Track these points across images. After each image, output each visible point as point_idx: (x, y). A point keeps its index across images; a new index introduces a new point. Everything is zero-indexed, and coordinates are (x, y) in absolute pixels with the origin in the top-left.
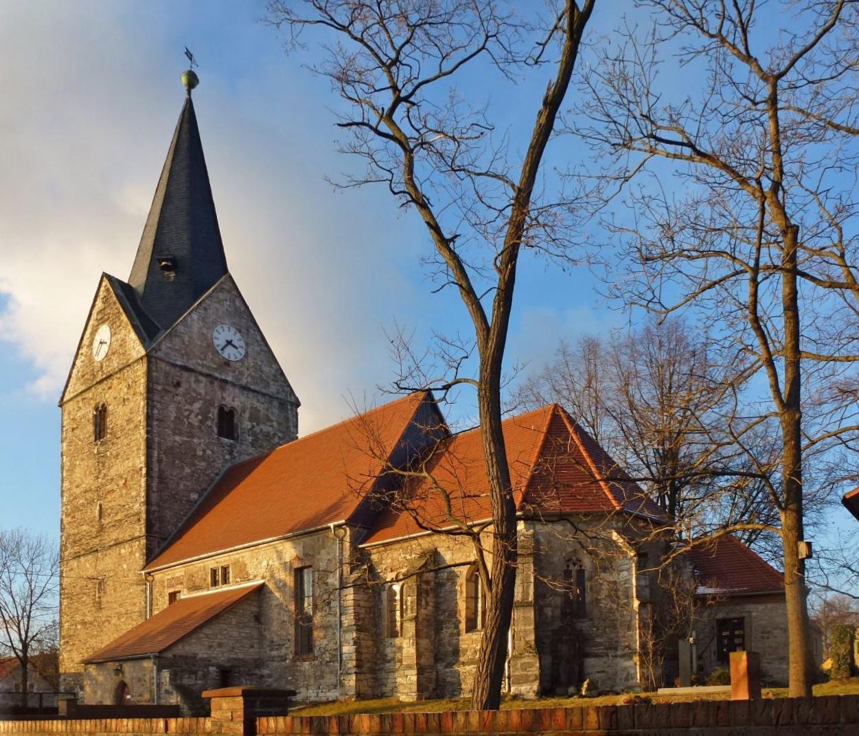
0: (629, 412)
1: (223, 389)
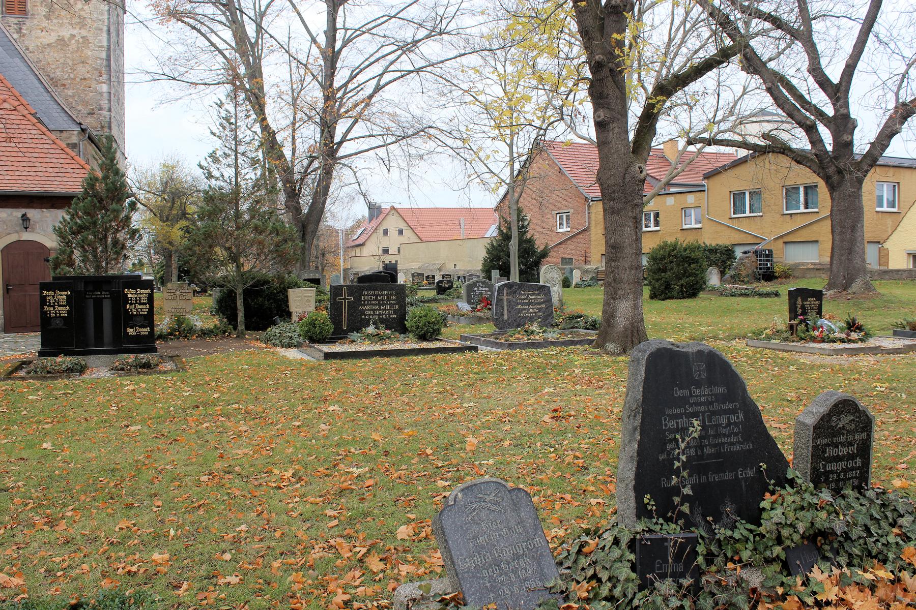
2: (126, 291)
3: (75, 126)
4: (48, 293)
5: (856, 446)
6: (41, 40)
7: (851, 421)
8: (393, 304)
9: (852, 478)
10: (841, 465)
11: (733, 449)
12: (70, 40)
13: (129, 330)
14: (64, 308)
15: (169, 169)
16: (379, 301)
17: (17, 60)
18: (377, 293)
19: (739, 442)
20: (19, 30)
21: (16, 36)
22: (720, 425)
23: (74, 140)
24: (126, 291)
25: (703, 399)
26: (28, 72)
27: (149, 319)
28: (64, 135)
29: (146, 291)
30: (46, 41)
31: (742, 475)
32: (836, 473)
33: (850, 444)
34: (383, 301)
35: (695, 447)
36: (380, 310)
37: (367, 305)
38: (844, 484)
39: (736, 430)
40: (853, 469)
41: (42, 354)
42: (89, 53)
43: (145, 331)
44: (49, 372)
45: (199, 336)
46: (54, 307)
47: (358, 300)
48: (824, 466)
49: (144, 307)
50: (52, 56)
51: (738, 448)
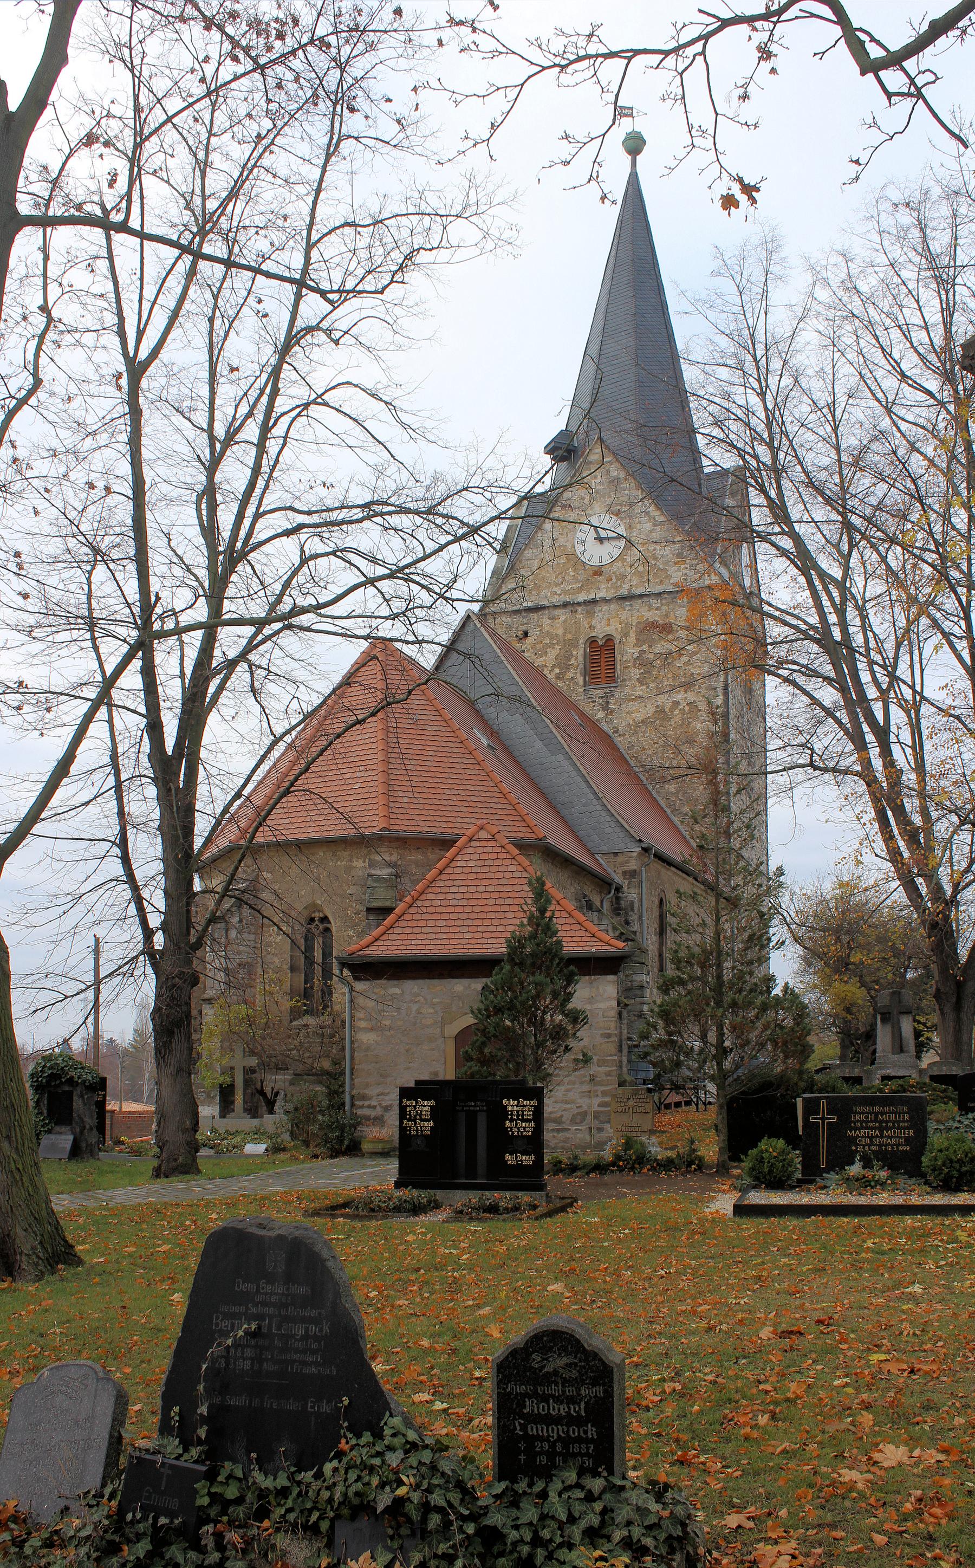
0: (889, 646)
1: (590, 614)
2: (505, 1102)
3: (633, 844)
4: (408, 1103)
5: (583, 1405)
6: (633, 716)
7: (569, 1365)
8: (904, 1128)
9: (580, 1454)
10: (556, 1431)
11: (306, 1371)
12: (672, 709)
13: (507, 1157)
14: (428, 1124)
15: (847, 888)
16: (881, 1122)
17: (561, 758)
18: (877, 1109)
19: (316, 1363)
20: (605, 707)
21: (601, 715)
22: (293, 1336)
23: (633, 865)
24: (505, 1102)
25: (274, 1299)
26: (574, 773)
27: (535, 1143)
28: (620, 859)
29: (531, 1103)
30: (639, 716)
31: (312, 1407)
32: (548, 1441)
33: (572, 1400)
34: (887, 1122)
35: (252, 1359)
36: (882, 1137)
37: (859, 1129)
38: (565, 1461)
39: (315, 1346)
40: (579, 1440)
41: (398, 1185)
42: (699, 726)
43: (528, 1160)
44: (373, 1210)
45: (653, 1169)
46: (415, 1121)
47: (845, 1121)
48: (524, 1428)
49: (528, 1125)
50: (647, 738)
51: (314, 1370)
